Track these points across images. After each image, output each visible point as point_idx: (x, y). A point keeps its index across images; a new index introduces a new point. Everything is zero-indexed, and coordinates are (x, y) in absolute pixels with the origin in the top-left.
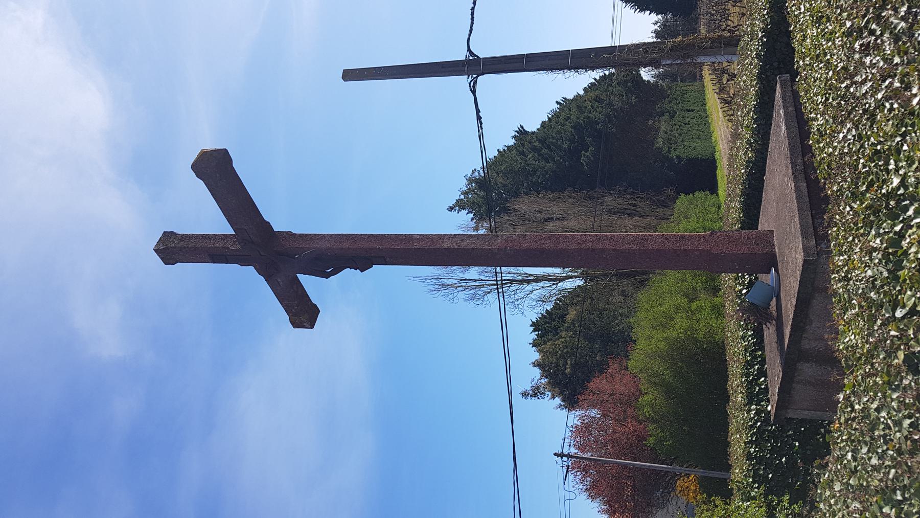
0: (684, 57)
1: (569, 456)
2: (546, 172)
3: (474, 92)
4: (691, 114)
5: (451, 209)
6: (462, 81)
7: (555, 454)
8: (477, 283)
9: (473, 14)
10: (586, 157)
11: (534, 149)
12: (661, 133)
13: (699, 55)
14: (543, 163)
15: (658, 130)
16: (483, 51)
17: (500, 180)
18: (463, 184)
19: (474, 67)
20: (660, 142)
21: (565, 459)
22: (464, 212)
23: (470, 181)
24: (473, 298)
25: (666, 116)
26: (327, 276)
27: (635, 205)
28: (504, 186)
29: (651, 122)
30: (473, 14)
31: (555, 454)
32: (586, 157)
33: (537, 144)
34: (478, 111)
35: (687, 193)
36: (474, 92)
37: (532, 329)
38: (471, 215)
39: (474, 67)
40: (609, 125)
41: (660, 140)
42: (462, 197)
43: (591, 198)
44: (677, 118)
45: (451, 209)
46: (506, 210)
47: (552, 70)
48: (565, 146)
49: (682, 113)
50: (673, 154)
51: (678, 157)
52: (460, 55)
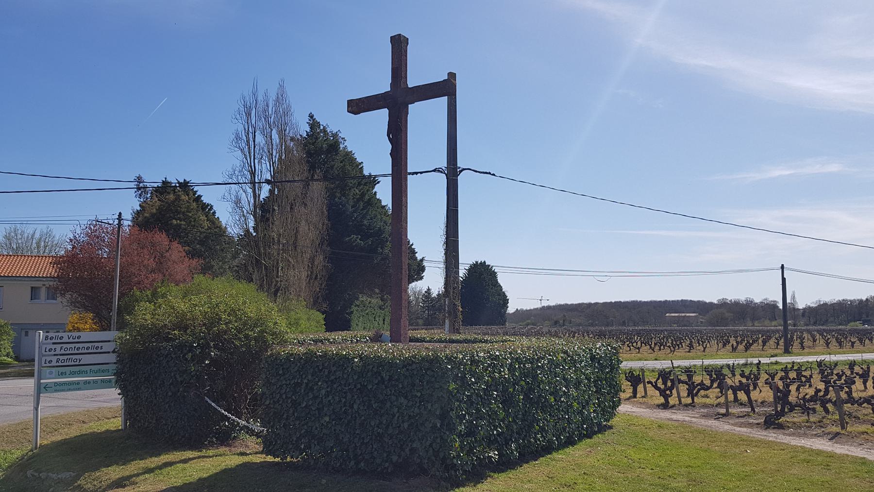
0: (449, 312)
1: (120, 225)
2: (344, 206)
3: (434, 171)
4: (381, 322)
5: (311, 116)
6: (443, 163)
7: (120, 213)
8: (251, 143)
9: (486, 173)
10: (356, 239)
11: (363, 195)
12: (369, 299)
13: (450, 321)
14: (351, 203)
15: (371, 297)
16: (463, 179)
17: (338, 164)
18: (332, 128)
19: (452, 172)
20: (363, 298)
21: (116, 222)
22: (308, 130)
23: (335, 135)
24: (238, 138)
25: (381, 303)
26: (388, 136)
27: (316, 278)
28: (332, 167)
29: (377, 291)
30: (486, 173)
31: (120, 213)
32: (356, 239)
33: (367, 197)
34: (421, 173)
35: (325, 319)
36: (434, 171)
37: (182, 181)
38: (305, 135)
39: (452, 172)
40: (379, 258)
41: (364, 299)
42: (322, 127)
43: (322, 243)
44: (379, 311)
45: (311, 116)
46: (312, 168)
47: (447, 226)
48: (365, 222)
49: (382, 315)
50: (354, 308)
51: (352, 312)
52: (461, 164)
